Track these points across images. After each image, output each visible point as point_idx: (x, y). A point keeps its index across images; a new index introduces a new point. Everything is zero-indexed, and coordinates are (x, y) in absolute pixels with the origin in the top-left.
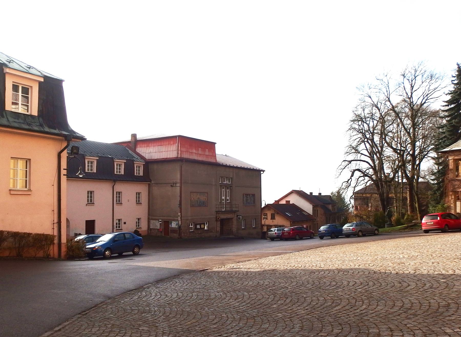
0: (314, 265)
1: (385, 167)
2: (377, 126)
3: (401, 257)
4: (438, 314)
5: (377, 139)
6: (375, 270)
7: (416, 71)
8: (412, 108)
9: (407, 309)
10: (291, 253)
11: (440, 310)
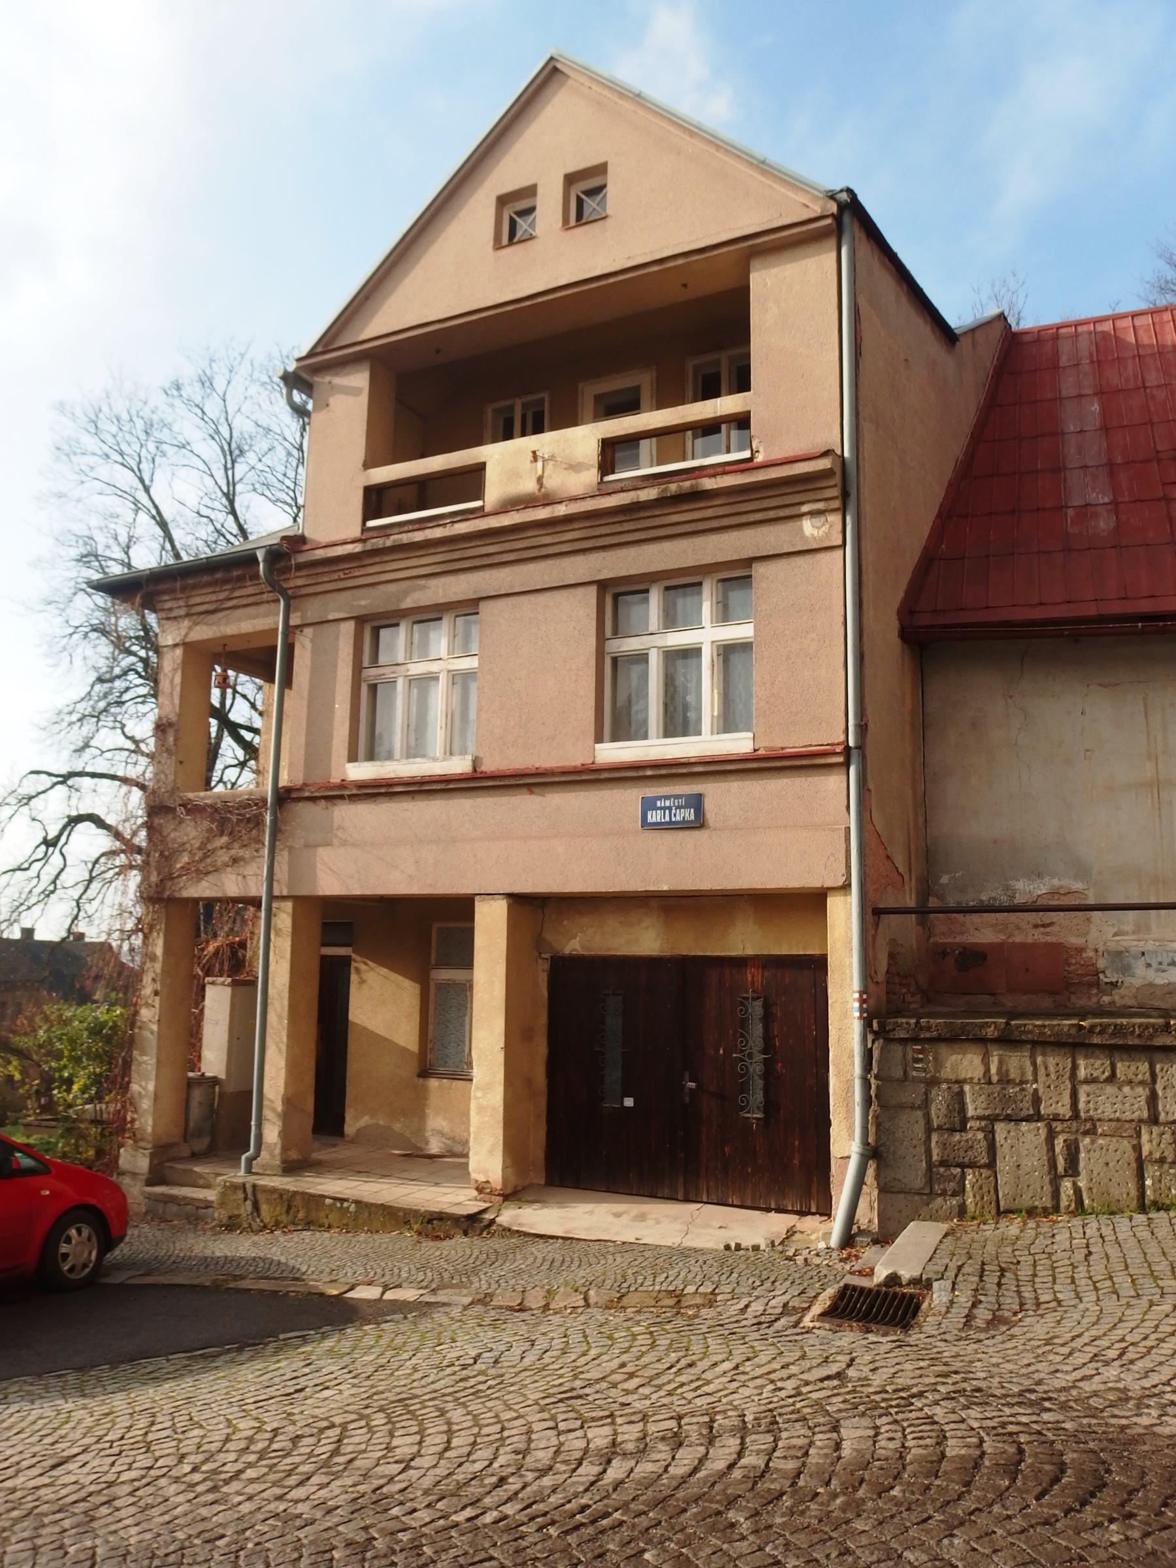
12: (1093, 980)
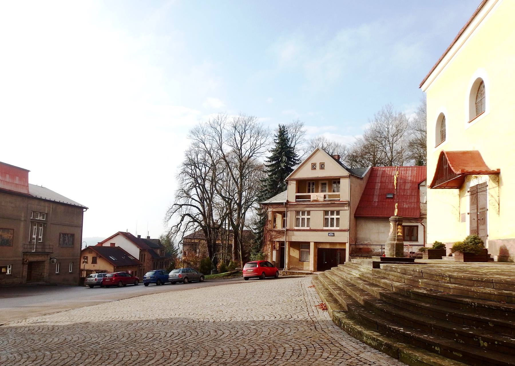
0: (133, 315)
1: (214, 214)
2: (208, 172)
3: (221, 304)
4: (245, 361)
5: (208, 185)
6: (194, 319)
7: (246, 126)
8: (241, 159)
9: (218, 358)
10: (110, 302)
11: (247, 357)
12: (371, 251)
